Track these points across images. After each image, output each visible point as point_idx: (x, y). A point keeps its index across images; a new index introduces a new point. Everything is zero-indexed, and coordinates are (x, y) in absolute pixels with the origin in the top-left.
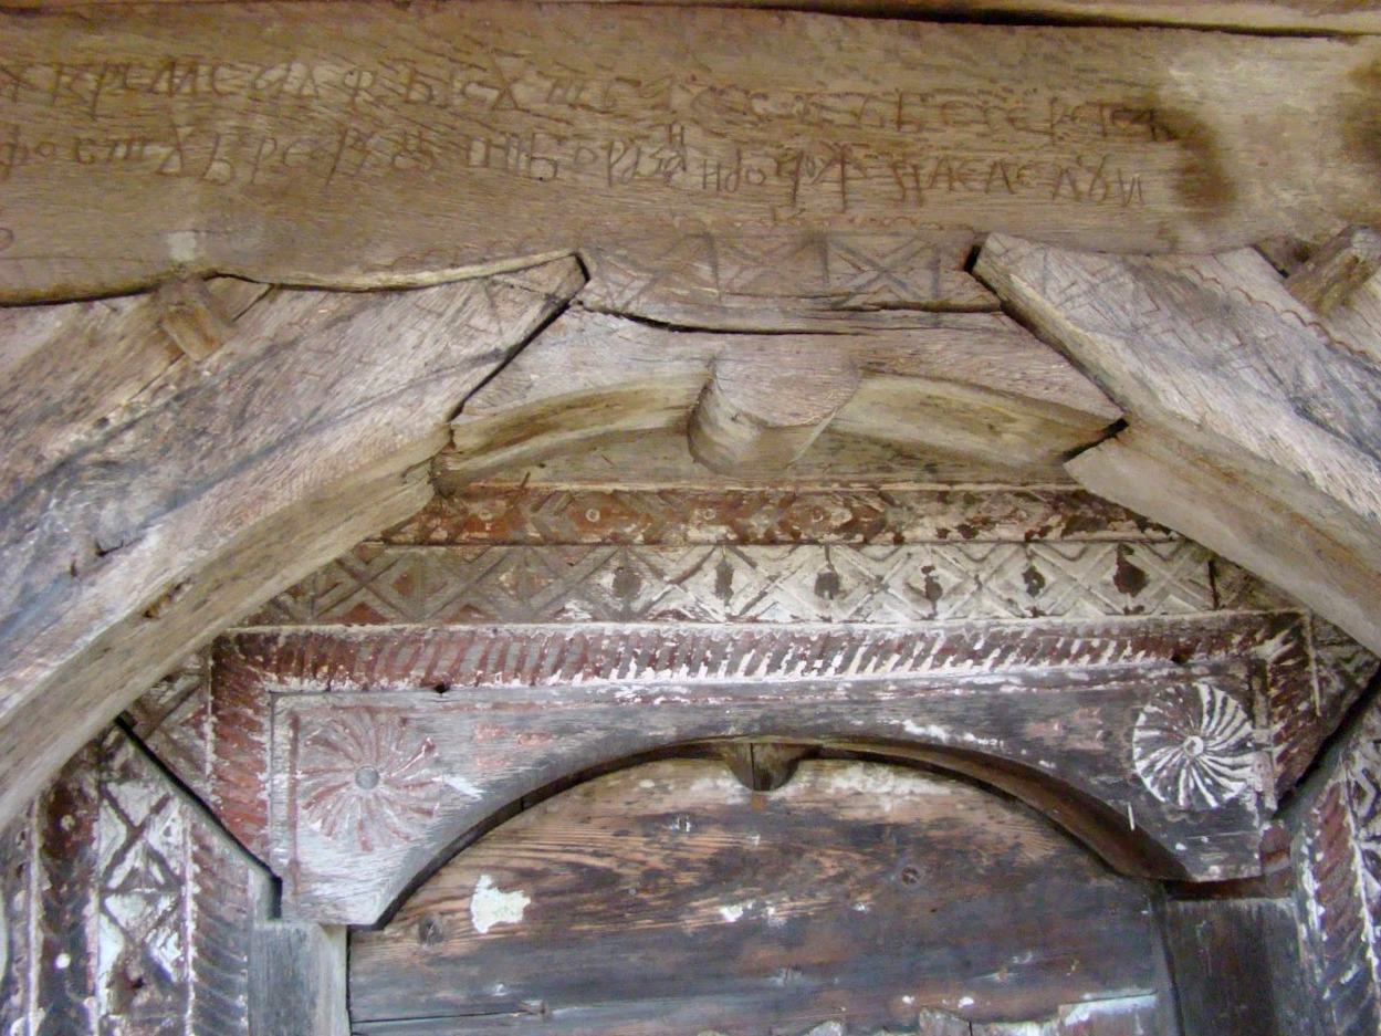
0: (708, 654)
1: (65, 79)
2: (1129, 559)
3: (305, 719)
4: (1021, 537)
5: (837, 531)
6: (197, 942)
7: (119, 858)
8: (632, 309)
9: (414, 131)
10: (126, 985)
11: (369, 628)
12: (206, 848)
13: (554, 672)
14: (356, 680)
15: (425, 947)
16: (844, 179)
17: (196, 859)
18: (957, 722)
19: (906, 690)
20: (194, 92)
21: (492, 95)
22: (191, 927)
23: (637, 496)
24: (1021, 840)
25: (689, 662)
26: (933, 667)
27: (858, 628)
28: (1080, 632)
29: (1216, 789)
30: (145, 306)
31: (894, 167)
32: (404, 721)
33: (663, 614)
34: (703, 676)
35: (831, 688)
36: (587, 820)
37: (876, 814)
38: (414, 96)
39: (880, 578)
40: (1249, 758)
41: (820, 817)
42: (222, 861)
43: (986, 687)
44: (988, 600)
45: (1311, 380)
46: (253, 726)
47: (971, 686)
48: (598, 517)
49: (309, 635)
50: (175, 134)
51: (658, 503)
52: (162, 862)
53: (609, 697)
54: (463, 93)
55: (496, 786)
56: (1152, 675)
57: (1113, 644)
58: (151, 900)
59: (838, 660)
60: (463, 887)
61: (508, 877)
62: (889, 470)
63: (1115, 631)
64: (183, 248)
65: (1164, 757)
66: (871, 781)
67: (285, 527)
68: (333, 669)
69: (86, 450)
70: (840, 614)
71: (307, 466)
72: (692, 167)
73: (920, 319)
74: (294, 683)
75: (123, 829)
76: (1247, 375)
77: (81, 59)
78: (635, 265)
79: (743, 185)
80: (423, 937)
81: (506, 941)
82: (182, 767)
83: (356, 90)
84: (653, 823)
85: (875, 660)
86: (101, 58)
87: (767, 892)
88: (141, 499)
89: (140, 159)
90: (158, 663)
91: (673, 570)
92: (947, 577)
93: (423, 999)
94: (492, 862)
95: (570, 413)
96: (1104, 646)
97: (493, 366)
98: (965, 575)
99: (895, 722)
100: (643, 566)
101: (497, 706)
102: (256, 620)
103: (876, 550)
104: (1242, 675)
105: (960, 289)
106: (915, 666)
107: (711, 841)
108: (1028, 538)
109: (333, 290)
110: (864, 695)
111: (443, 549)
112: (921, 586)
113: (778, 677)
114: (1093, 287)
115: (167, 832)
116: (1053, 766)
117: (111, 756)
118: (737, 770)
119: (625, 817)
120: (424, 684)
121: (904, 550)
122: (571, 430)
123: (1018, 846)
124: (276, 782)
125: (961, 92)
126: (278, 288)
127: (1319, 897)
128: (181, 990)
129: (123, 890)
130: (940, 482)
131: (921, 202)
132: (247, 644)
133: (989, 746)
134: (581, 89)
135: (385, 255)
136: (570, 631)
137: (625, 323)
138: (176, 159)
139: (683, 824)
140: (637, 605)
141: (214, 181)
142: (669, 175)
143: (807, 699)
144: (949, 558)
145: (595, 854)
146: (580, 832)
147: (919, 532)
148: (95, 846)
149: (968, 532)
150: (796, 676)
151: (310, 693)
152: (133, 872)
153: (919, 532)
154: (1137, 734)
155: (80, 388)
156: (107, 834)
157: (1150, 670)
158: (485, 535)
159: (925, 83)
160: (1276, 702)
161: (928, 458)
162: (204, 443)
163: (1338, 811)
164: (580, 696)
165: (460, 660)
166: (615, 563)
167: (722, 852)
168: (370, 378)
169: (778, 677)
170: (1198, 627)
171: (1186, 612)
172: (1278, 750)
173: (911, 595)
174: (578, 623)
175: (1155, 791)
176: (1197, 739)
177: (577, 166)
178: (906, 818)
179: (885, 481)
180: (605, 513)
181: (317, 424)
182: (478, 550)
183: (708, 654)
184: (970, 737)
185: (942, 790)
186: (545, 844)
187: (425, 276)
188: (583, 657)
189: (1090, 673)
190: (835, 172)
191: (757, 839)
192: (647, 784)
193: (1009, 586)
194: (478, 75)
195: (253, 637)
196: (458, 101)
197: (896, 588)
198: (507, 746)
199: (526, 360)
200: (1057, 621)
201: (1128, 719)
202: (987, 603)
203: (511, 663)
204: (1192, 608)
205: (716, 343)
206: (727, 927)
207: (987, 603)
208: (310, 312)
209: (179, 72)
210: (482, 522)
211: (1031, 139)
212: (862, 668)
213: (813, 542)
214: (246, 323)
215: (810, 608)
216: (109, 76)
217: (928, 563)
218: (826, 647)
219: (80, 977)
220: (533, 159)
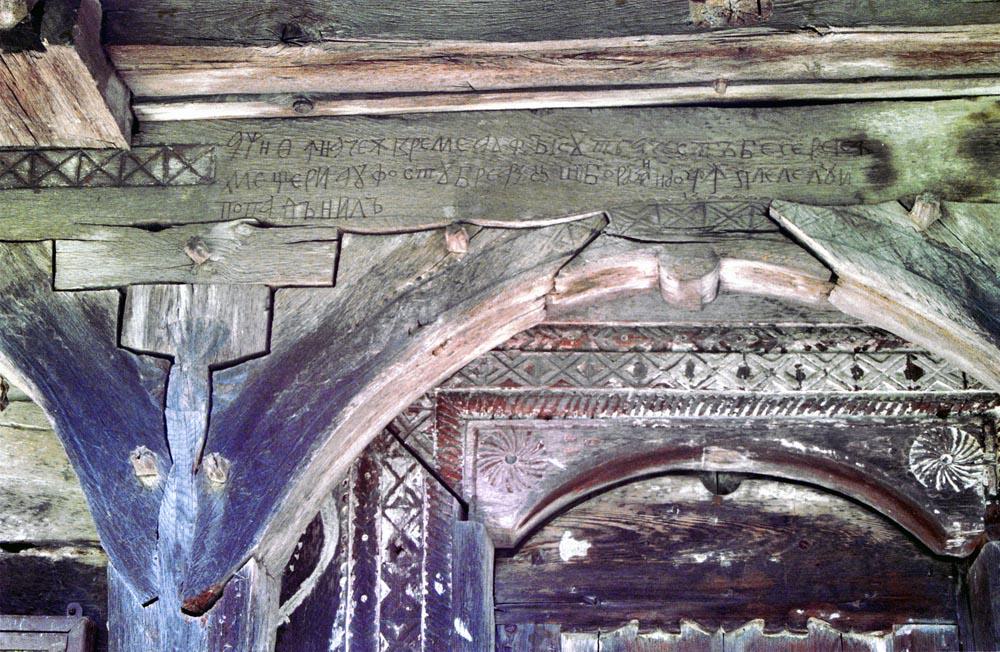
0: (680, 404)
1: (398, 145)
2: (914, 362)
3: (481, 431)
4: (853, 350)
6: (428, 529)
7: (392, 492)
8: (625, 234)
9: (539, 164)
10: (394, 550)
11: (513, 389)
12: (434, 488)
13: (603, 411)
14: (507, 414)
15: (535, 566)
17: (428, 492)
20: (450, 151)
21: (572, 149)
22: (425, 523)
23: (647, 329)
24: (872, 530)
25: (670, 407)
26: (798, 414)
27: (759, 394)
28: (882, 399)
29: (959, 483)
30: (434, 235)
31: (738, 173)
33: (658, 385)
34: (677, 414)
35: (744, 421)
37: (784, 510)
38: (540, 151)
39: (772, 370)
42: (441, 493)
43: (826, 424)
45: (916, 254)
46: (456, 433)
47: (818, 423)
48: (627, 339)
49: (484, 393)
50: (443, 167)
51: (659, 333)
52: (412, 493)
54: (559, 148)
56: (923, 422)
57: (900, 405)
58: (407, 510)
59: (747, 408)
60: (555, 537)
61: (580, 532)
62: (780, 316)
63: (903, 399)
65: (927, 463)
68: (496, 407)
69: (413, 289)
72: (653, 178)
73: (743, 237)
74: (476, 414)
75: (394, 479)
77: (404, 136)
79: (673, 184)
80: (533, 561)
81: (577, 565)
82: (423, 452)
83: (516, 149)
85: (767, 409)
86: (412, 136)
87: (720, 548)
88: (435, 305)
89: (430, 177)
90: (430, 381)
91: (664, 365)
92: (808, 369)
93: (532, 592)
94: (571, 524)
95: (603, 278)
97: (571, 256)
99: (776, 440)
100: (649, 362)
103: (771, 356)
107: (690, 519)
108: (857, 351)
111: (549, 353)
112: (794, 374)
114: (817, 220)
115: (415, 481)
116: (863, 466)
117: (388, 446)
118: (708, 485)
119: (643, 505)
120: (539, 417)
121: (786, 356)
122: (606, 287)
124: (467, 460)
125: (771, 138)
128: (420, 552)
129: (393, 506)
130: (807, 322)
132: (455, 396)
133: (828, 455)
134: (607, 146)
137: (622, 239)
138: (445, 177)
139: (675, 510)
140: (645, 381)
141: (461, 186)
142: (642, 181)
144: (810, 360)
145: (627, 523)
148: (380, 487)
151: (483, 419)
152: (399, 498)
155: (410, 265)
156: (386, 480)
157: (922, 419)
158: (570, 347)
159: (755, 135)
161: (802, 310)
164: (616, 422)
166: (635, 361)
167: (696, 526)
168: (522, 262)
170: (953, 399)
171: (946, 389)
173: (788, 378)
175: (922, 481)
176: (949, 456)
177: (605, 178)
178: (802, 513)
179: (777, 322)
180: (630, 337)
182: (567, 354)
183: (680, 404)
185: (825, 499)
188: (618, 403)
189: (885, 419)
190: (713, 176)
191: (716, 520)
194: (565, 141)
195: (457, 394)
196: (557, 152)
199: (584, 254)
200: (870, 392)
201: (907, 444)
202: (829, 382)
204: (951, 388)
205: (658, 247)
206: (697, 565)
207: (829, 382)
208: (499, 237)
209: (444, 141)
211: (801, 158)
213: (739, 352)
216: (416, 143)
217: (798, 362)
219: (373, 544)
220: (587, 175)
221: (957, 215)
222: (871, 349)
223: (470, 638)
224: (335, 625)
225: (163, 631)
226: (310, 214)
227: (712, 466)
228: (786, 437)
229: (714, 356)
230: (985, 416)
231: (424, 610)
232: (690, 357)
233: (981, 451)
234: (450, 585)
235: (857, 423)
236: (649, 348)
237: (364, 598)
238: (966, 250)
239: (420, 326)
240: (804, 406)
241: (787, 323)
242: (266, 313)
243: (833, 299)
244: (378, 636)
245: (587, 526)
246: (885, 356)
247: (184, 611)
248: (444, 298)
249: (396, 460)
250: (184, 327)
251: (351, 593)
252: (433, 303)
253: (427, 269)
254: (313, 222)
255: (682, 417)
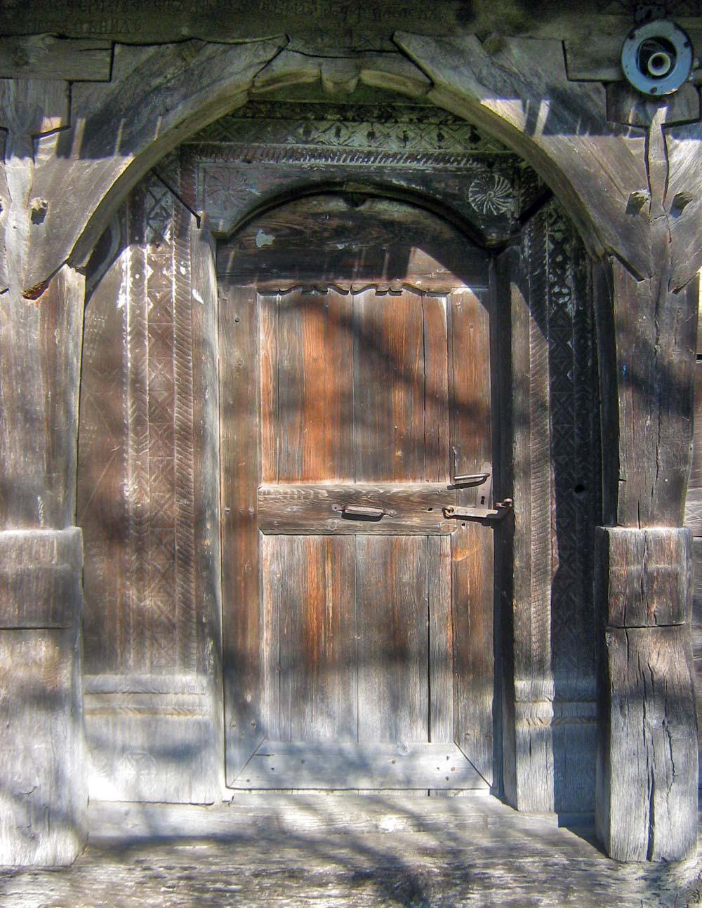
2: (475, 132)
5: (376, 118)
7: (153, 209)
11: (228, 143)
16: (359, 15)
18: (409, 181)
19: (393, 169)
27: (380, 150)
29: (497, 209)
32: (238, 172)
35: (370, 167)
36: (294, 213)
37: (391, 218)
40: (510, 200)
41: (371, 217)
44: (424, 143)
45: (484, 72)
46: (194, 172)
47: (415, 169)
53: (300, 167)
55: (266, 192)
57: (465, 159)
59: (372, 159)
64: (185, 31)
65: (479, 197)
66: (391, 206)
67: (211, 106)
70: (374, 144)
71: (218, 89)
74: (204, 159)
76: (466, 72)
78: (302, 39)
80: (240, 248)
84: (316, 215)
87: (353, 240)
88: (177, 97)
92: (411, 134)
96: (462, 160)
97: (262, 66)
98: (417, 134)
101: (266, 168)
102: (193, 140)
104: (511, 173)
105: (388, 45)
106: (398, 162)
107: (336, 222)
108: (441, 123)
109: (224, 43)
110: (380, 170)
113: (353, 163)
114: (423, 46)
117: (150, 179)
118: (346, 200)
120: (244, 161)
123: (441, 233)
124: (199, 189)
126: (209, 42)
127: (530, 247)
129: (154, 218)
131: (380, 21)
132: (190, 146)
135: (235, 35)
136: (289, 147)
137: (298, 54)
140: (310, 139)
142: (311, 13)
143: (362, 170)
145: (298, 225)
146: (291, 217)
147: (403, 119)
149: (420, 120)
150: (359, 163)
152: (157, 213)
153: (403, 119)
154: (471, 189)
156: (149, 202)
160: (523, 183)
162: (192, 83)
163: (542, 221)
164: (291, 166)
165: (255, 154)
167: (338, 226)
169: (353, 163)
170: (497, 155)
172: (522, 199)
174: (291, 144)
175: (475, 208)
181: (220, 79)
184: (414, 186)
185: (416, 211)
186: (281, 220)
187: (248, 40)
188: (293, 154)
192: (315, 203)
193: (431, 138)
195: (192, 145)
197: (393, 138)
198: (268, 181)
199: (273, 63)
202: (423, 143)
203: (270, 155)
205: (321, 60)
207: (423, 143)
208: (218, 49)
210: (267, 112)
212: (380, 162)
213: (367, 121)
214: (202, 52)
215: (365, 142)
218: (369, 154)
221: (511, 46)
222: (449, 122)
223: (202, 301)
224: (120, 292)
225: (13, 310)
226: (93, 30)
227: (349, 190)
228: (396, 178)
229: (353, 124)
230: (515, 168)
231: (174, 284)
232: (338, 124)
233: (511, 190)
234: (190, 269)
235: (440, 170)
236: (313, 117)
237: (137, 276)
238: (516, 71)
239: (167, 110)
240: (407, 158)
241: (399, 104)
242: (66, 100)
243: (430, 95)
244: (147, 299)
245: (272, 226)
246: (458, 127)
247: (26, 297)
248: (183, 91)
249: (155, 188)
250: (13, 109)
251: (129, 272)
252: (175, 95)
253: (171, 70)
254: (95, 36)
255: (332, 163)
